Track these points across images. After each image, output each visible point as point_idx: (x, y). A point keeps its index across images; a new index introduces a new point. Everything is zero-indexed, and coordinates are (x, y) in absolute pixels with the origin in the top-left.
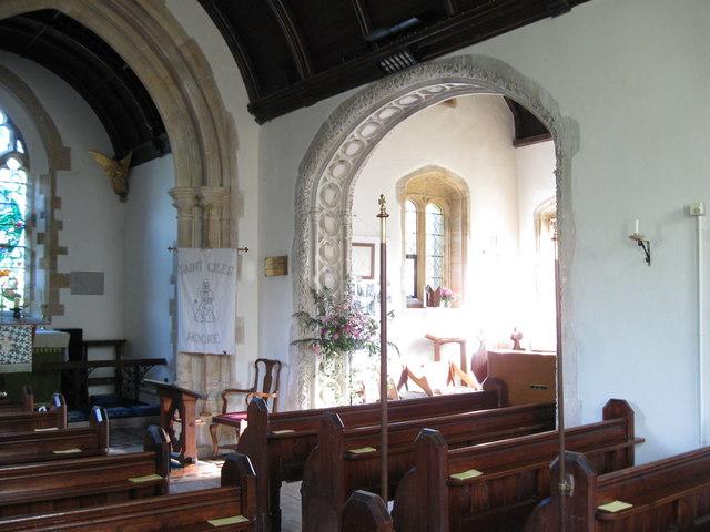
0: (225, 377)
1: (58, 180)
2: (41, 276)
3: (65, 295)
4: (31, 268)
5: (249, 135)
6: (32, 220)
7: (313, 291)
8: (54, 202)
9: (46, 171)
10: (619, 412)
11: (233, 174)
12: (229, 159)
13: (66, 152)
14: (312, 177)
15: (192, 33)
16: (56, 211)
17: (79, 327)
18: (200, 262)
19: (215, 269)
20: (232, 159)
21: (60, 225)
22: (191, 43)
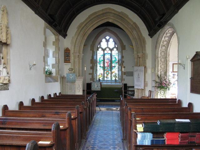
0: (143, 94)
1: (123, 52)
2: (120, 72)
3: (124, 77)
4: (119, 71)
5: (149, 41)
6: (119, 61)
7: (158, 76)
8: (122, 57)
9: (121, 51)
10: (190, 105)
11: (145, 50)
12: (144, 47)
13: (125, 46)
14: (157, 50)
15: (134, 21)
16: (123, 59)
17: (126, 83)
18: (138, 69)
19: (140, 71)
20: (145, 47)
21: (124, 62)
22: (135, 23)
